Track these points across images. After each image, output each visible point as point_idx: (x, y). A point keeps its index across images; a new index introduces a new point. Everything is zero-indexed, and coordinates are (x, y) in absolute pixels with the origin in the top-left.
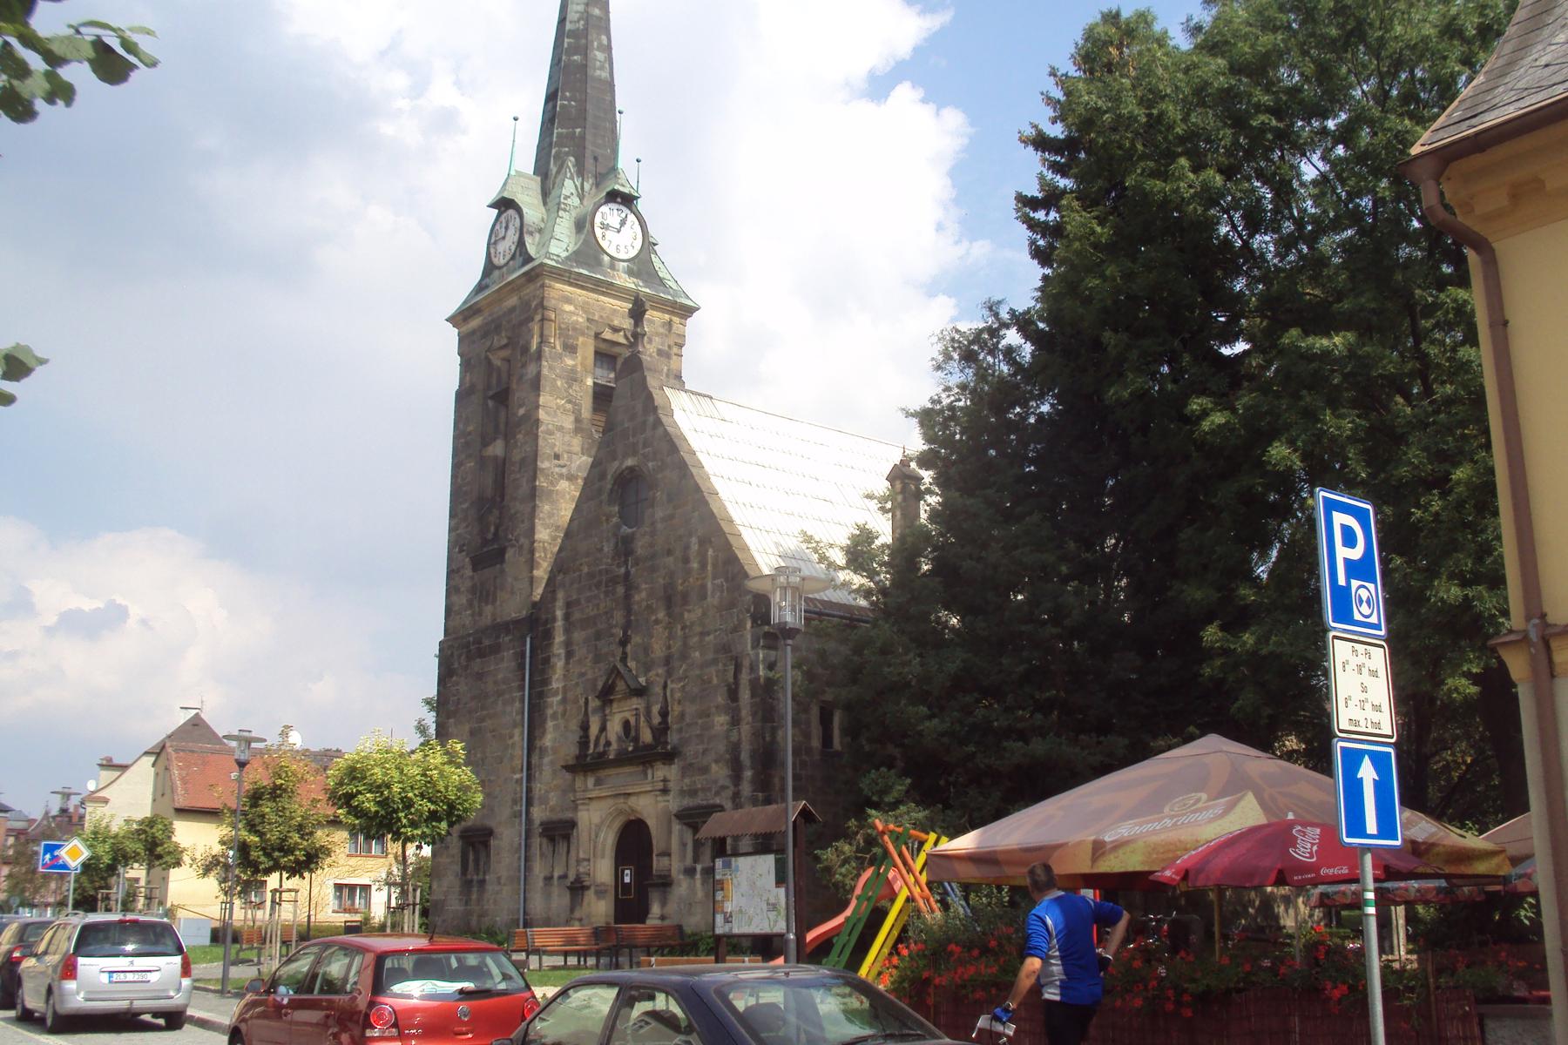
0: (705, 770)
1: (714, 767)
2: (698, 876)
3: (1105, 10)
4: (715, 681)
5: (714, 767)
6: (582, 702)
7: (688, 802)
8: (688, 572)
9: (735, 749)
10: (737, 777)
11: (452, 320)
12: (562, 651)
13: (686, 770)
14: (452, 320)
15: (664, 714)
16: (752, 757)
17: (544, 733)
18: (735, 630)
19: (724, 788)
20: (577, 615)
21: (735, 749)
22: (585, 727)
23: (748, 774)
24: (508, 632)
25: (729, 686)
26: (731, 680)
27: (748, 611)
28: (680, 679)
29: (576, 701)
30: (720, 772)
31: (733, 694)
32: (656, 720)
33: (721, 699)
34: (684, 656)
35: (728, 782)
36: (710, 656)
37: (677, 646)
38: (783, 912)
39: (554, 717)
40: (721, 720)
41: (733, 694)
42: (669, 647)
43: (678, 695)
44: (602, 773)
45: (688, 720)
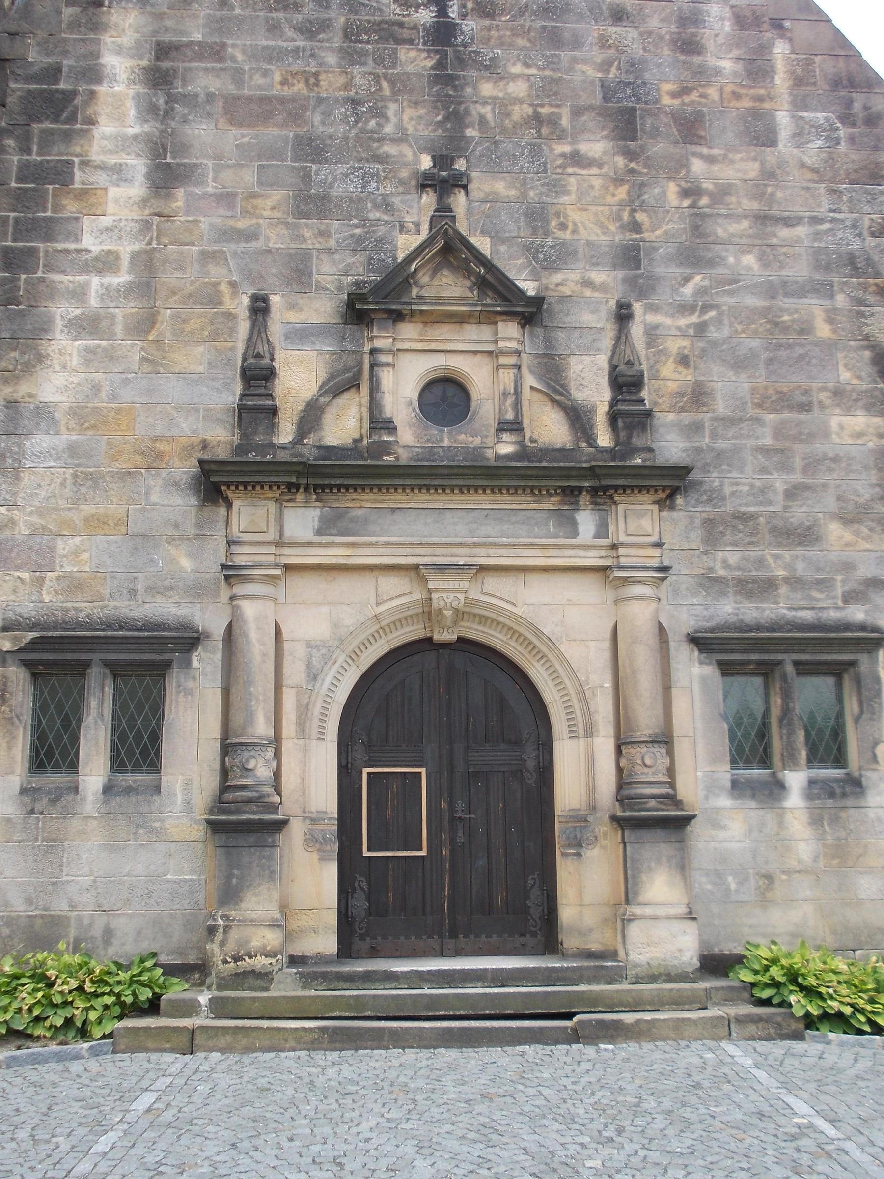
12: (138, 165)
37: (664, 230)
39: (88, 325)
43: (675, 345)
44: (344, 502)
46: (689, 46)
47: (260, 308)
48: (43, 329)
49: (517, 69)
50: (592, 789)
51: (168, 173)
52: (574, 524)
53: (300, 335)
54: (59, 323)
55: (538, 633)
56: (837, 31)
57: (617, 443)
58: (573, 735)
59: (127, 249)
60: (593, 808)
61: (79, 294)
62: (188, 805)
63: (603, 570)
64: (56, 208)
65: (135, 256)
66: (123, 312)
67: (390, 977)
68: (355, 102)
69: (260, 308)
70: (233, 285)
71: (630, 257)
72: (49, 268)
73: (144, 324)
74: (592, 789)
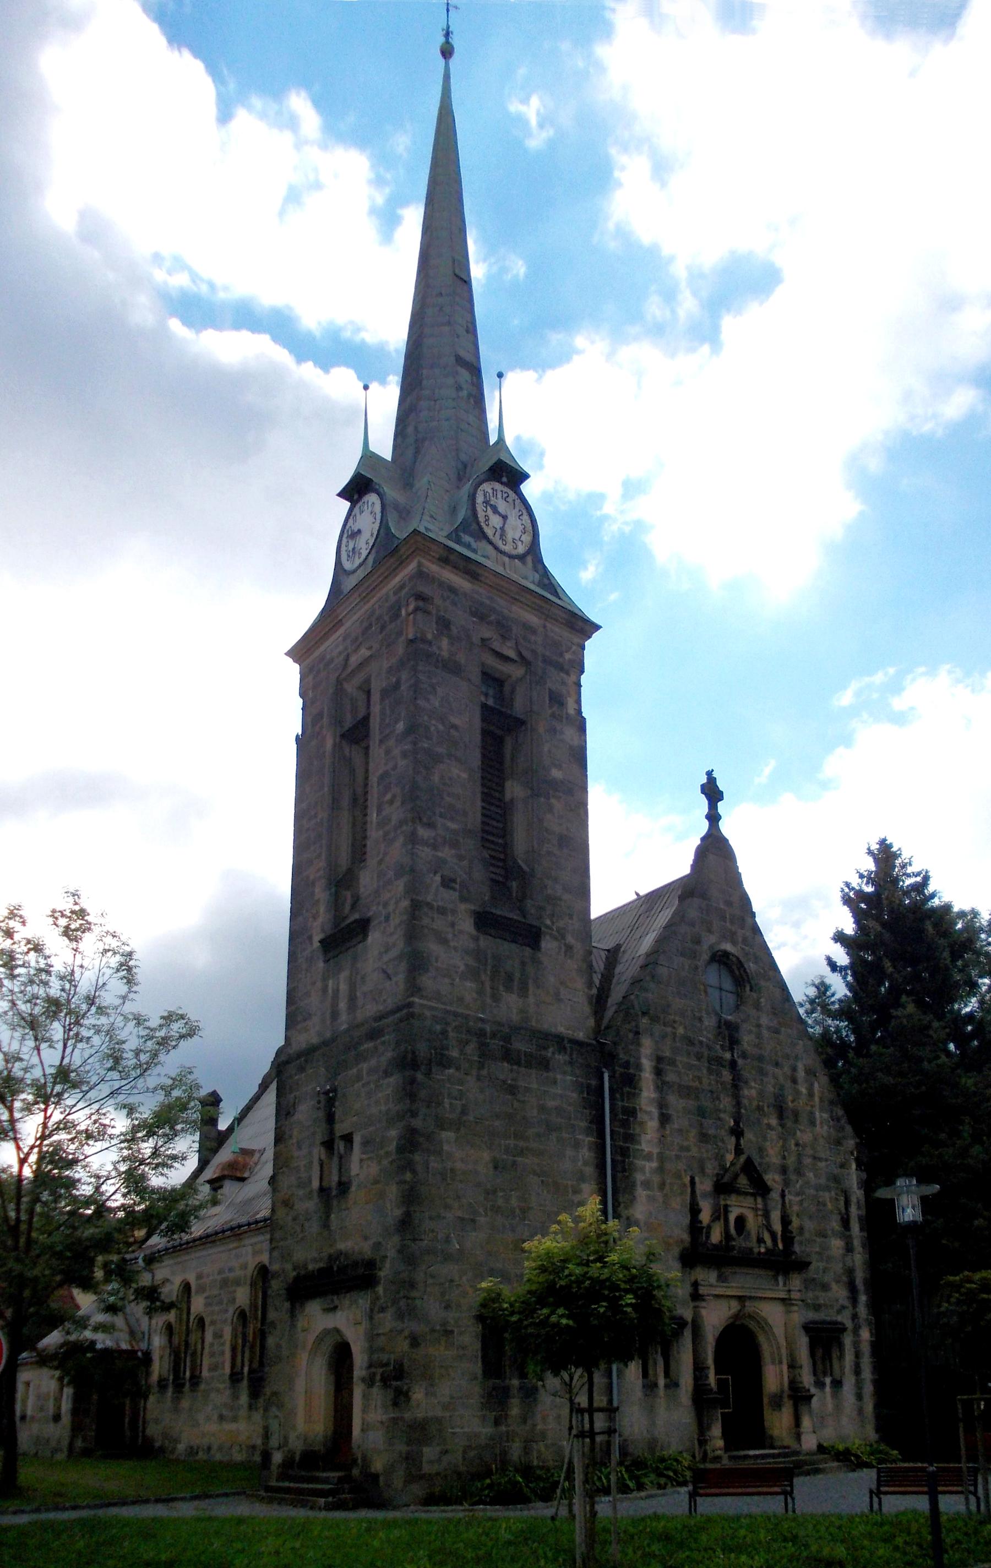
0: (825, 1287)
1: (834, 1286)
2: (828, 1389)
3: (832, 935)
4: (829, 1206)
5: (834, 1286)
6: (687, 1180)
7: (812, 1315)
8: (798, 1093)
9: (850, 1272)
10: (854, 1300)
11: (290, 653)
12: (655, 1111)
13: (809, 1284)
14: (290, 653)
15: (786, 1221)
16: (865, 1284)
17: (633, 1200)
18: (842, 1166)
19: (843, 1307)
20: (671, 1077)
21: (850, 1272)
22: (695, 1211)
23: (863, 1298)
24: (562, 1049)
25: (842, 1218)
26: (843, 1211)
27: (852, 1153)
28: (798, 1194)
29: (678, 1176)
30: (839, 1293)
31: (846, 1222)
32: (778, 1227)
33: (835, 1224)
34: (799, 1173)
35: (847, 1303)
36: (823, 1181)
37: (791, 1161)
38: (206, 1350)
39: (647, 1185)
40: (837, 1245)
41: (846, 1222)
42: (784, 1158)
43: (796, 1208)
44: (728, 1271)
45: (807, 1235)
46: (794, 1081)
47: (693, 1182)
48: (633, 1185)
49: (753, 1084)
50: (782, 1384)
51: (664, 1119)
52: (777, 1280)
53: (704, 1195)
54: (638, 1183)
55: (767, 1323)
56: (288, 1028)
57: (145, 1188)
58: (773, 1363)
59: (655, 1151)
60: (782, 1392)
61: (642, 1170)
62: (687, 1391)
63: (783, 1300)
64: (634, 1129)
65: (658, 1154)
66: (656, 1179)
67: (746, 1457)
68: (712, 1092)
69: (693, 1182)
70: (685, 1171)
71: (784, 1170)
72: (634, 1158)
73: (662, 1185)
74: (782, 1384)
